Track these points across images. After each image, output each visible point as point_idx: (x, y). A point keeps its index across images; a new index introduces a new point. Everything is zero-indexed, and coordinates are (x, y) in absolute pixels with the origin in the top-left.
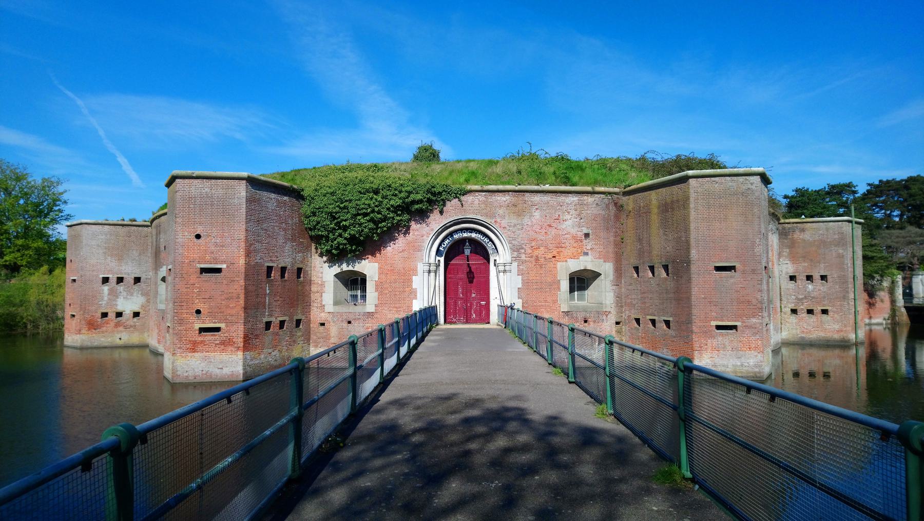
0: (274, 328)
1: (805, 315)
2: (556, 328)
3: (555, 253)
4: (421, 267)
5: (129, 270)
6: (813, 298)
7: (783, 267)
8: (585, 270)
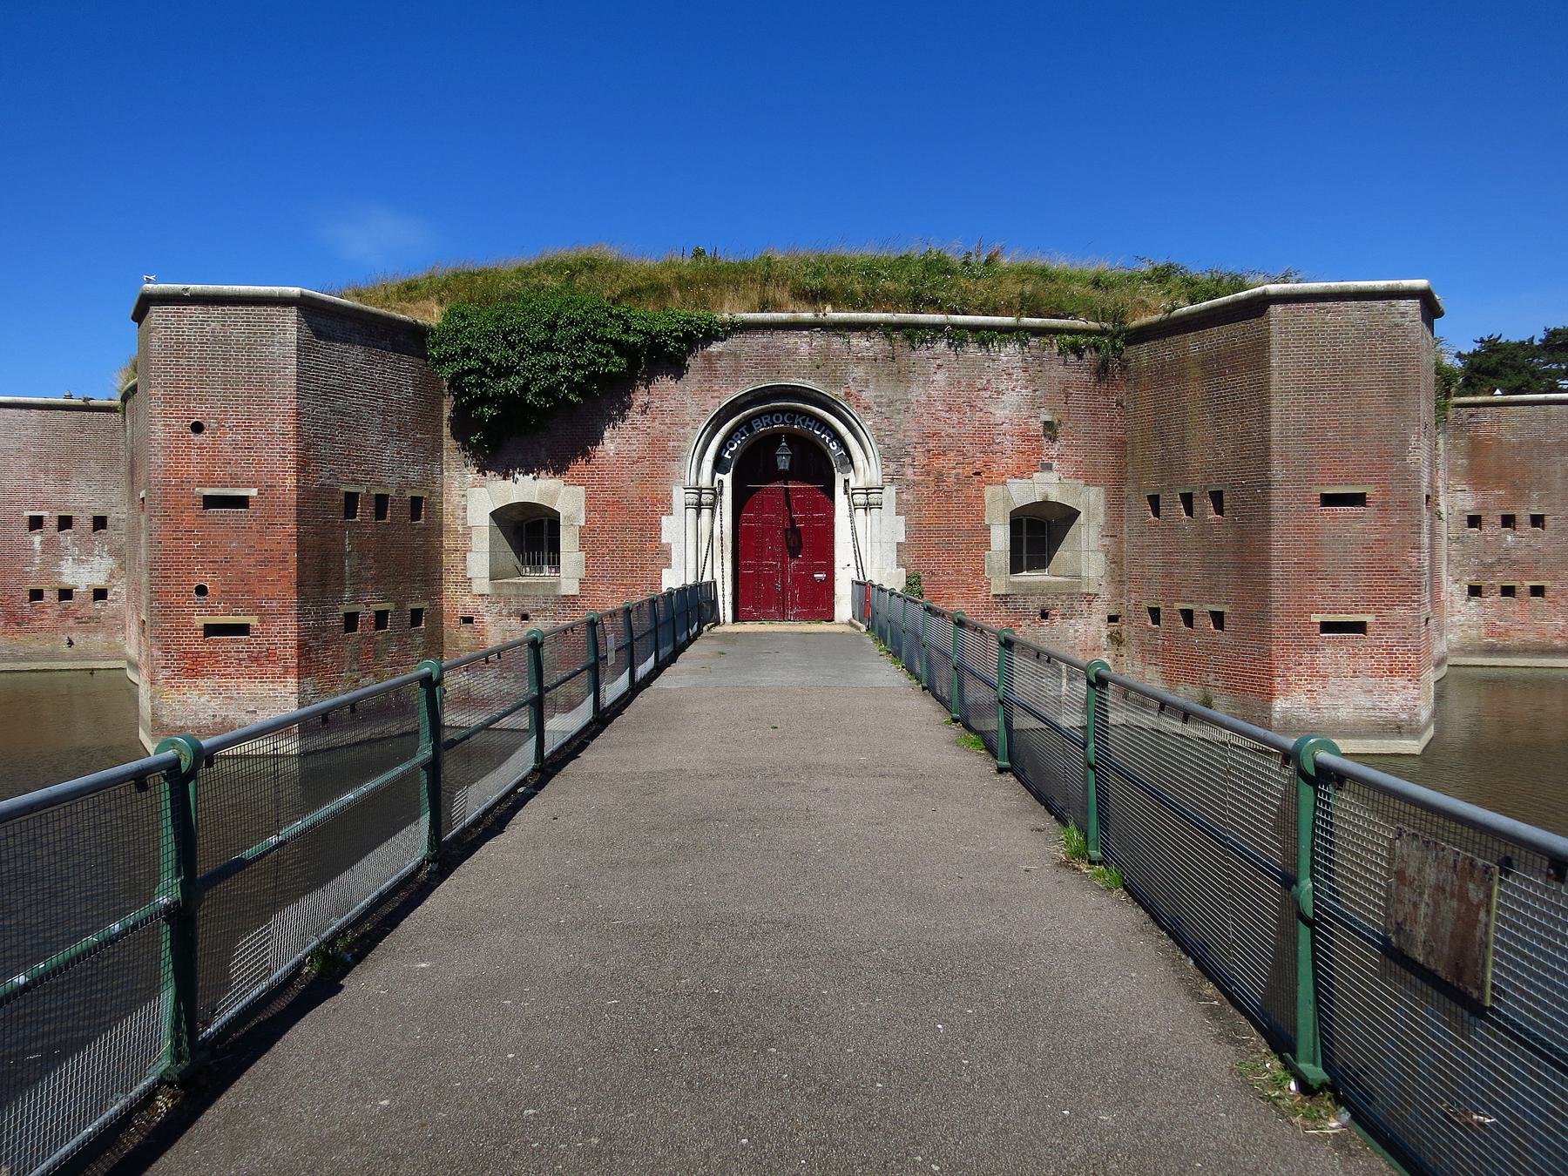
0: (364, 628)
1: (1497, 597)
2: (969, 636)
3: (978, 464)
4: (679, 497)
5: (83, 500)
6: (1516, 562)
7: (1456, 500)
8: (1045, 504)
